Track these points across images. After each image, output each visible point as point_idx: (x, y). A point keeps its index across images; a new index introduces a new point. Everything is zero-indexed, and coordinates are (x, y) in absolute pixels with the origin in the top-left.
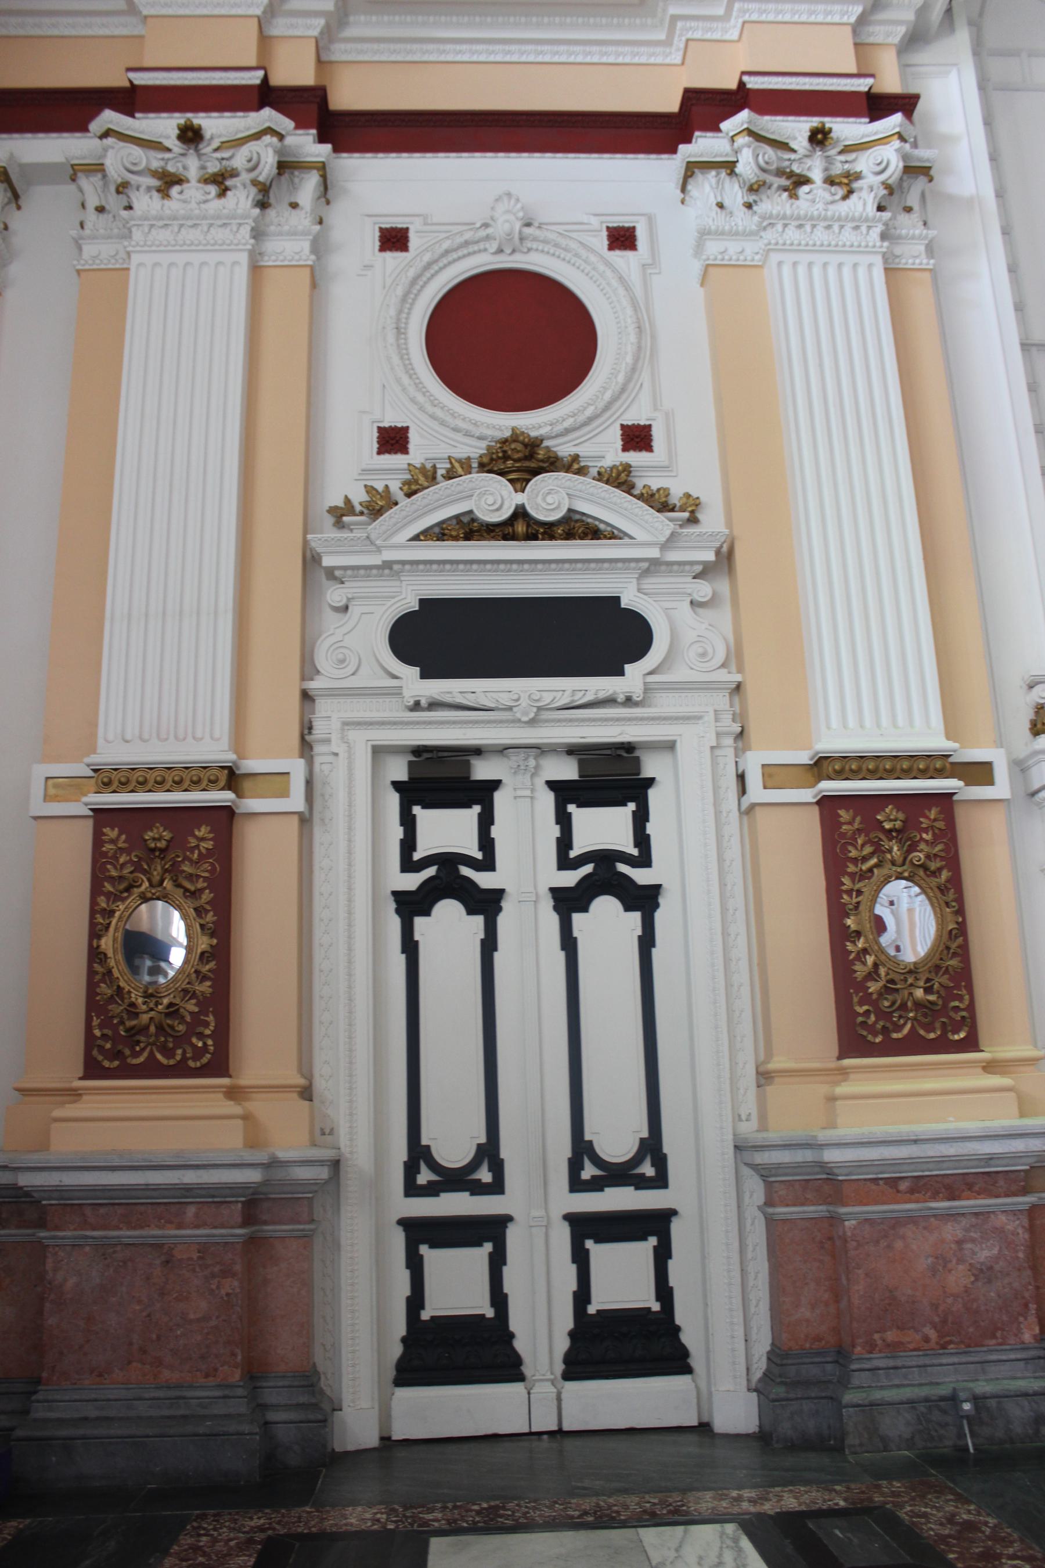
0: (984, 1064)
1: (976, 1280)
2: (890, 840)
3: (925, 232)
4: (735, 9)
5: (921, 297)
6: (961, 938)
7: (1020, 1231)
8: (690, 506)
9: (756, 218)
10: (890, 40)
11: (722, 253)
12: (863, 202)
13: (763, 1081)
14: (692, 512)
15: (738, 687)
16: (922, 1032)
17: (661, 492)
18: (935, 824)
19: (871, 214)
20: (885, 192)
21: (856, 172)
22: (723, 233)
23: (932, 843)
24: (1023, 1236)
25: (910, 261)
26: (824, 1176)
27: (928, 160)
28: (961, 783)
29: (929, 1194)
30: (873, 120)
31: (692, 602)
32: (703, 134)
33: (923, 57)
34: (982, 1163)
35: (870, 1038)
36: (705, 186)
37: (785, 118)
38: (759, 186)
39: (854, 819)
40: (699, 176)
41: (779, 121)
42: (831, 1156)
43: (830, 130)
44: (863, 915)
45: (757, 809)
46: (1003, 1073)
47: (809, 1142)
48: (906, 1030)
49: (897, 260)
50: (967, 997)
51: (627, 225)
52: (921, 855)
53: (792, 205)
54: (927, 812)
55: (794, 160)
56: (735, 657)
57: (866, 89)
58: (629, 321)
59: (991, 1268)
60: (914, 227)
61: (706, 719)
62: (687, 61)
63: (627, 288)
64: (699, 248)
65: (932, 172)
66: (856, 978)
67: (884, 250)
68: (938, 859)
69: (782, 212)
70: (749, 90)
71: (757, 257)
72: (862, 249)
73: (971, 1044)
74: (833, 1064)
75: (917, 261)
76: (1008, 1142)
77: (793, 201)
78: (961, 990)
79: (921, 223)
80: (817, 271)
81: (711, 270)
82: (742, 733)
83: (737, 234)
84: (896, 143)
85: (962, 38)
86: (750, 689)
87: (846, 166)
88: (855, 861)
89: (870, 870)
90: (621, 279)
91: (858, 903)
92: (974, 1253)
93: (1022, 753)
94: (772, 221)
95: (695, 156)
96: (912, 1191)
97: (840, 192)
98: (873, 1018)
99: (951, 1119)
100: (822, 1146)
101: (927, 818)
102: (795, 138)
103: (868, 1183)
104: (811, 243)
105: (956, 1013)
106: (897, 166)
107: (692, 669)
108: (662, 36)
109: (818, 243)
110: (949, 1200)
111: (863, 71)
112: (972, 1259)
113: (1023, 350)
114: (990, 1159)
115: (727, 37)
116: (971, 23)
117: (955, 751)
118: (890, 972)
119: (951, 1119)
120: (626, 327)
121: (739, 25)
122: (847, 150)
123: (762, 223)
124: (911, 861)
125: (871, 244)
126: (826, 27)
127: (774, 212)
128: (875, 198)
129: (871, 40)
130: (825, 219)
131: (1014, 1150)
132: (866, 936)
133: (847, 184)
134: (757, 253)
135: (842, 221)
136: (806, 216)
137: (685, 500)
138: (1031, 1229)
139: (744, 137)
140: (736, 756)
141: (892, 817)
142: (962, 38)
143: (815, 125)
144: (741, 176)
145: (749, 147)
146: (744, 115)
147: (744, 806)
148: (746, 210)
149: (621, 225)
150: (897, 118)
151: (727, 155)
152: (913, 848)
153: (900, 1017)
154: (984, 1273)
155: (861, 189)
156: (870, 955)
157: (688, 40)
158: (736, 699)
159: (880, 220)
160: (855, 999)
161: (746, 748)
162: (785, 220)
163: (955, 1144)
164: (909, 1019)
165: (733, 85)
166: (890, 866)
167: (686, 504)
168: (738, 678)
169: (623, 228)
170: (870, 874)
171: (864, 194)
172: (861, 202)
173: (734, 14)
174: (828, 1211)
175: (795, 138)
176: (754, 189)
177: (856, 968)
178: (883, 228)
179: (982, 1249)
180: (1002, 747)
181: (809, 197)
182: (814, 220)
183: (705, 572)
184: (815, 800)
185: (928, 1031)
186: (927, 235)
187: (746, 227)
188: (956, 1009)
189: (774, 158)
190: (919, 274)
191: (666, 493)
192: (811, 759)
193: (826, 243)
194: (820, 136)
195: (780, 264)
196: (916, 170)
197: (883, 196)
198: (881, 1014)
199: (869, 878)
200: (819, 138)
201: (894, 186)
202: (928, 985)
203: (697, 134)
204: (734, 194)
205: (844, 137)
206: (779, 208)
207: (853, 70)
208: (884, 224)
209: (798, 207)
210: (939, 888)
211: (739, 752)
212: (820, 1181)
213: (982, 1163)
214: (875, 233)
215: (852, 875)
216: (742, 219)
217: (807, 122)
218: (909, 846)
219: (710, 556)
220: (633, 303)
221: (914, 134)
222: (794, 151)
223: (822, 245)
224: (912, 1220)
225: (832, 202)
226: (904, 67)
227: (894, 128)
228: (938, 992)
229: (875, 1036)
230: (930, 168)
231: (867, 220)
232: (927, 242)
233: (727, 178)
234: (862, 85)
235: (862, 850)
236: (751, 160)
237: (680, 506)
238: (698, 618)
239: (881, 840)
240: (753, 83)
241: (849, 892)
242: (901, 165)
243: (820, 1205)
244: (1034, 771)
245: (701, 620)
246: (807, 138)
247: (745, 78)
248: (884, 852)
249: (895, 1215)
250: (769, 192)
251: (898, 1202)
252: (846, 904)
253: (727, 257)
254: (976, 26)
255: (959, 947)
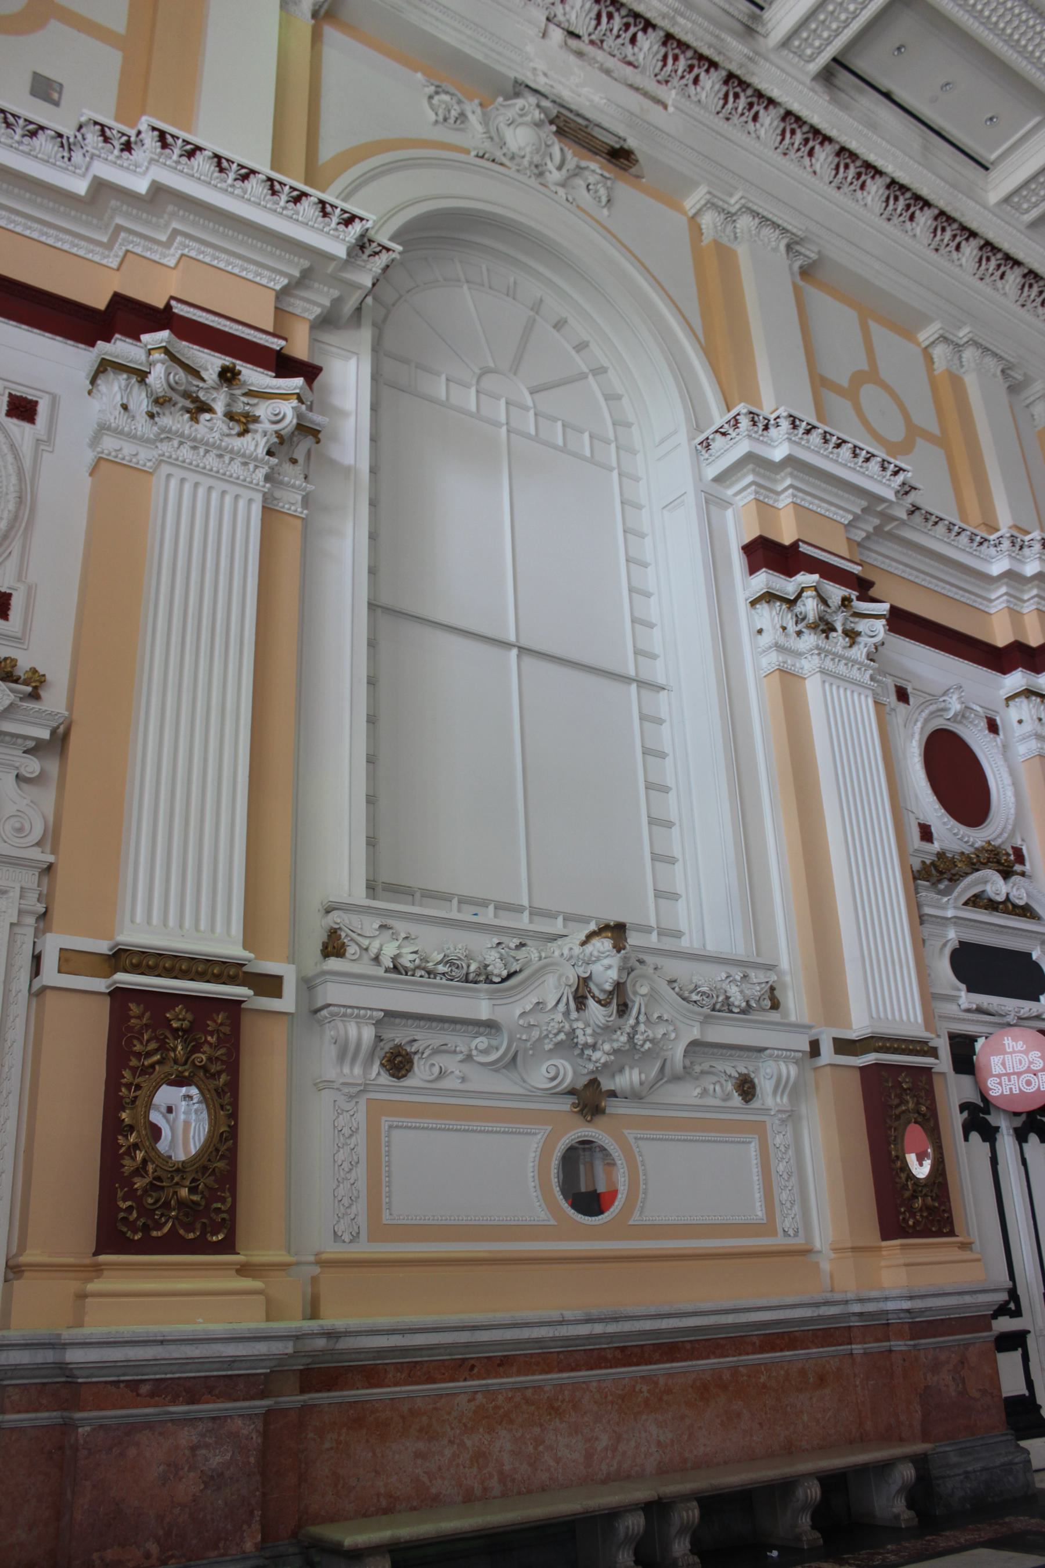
0: (239, 1267)
1: (206, 1487)
2: (176, 1039)
3: (304, 484)
4: (177, 241)
5: (290, 539)
6: (232, 1141)
7: (254, 1435)
8: (35, 681)
9: (156, 429)
10: (306, 315)
11: (116, 451)
12: (255, 444)
13: (11, 1275)
14: (35, 688)
15: (49, 869)
16: (182, 1232)
17: (8, 662)
18: (221, 1028)
19: (260, 456)
20: (276, 440)
21: (254, 416)
22: (121, 433)
23: (216, 1046)
24: (257, 1439)
25: (287, 506)
26: (63, 1379)
27: (318, 424)
28: (251, 992)
29: (169, 1398)
30: (278, 376)
31: (17, 776)
32: (123, 338)
33: (332, 338)
34: (226, 1366)
35: (129, 1234)
36: (114, 387)
37: (202, 349)
38: (165, 401)
39: (143, 1014)
40: (111, 374)
41: (196, 350)
42: (74, 1356)
43: (239, 373)
44: (140, 1109)
45: (48, 992)
46: (254, 1277)
47: (52, 1341)
48: (166, 1229)
49: (275, 502)
50: (229, 1200)
51: (30, 397)
52: (204, 1057)
53: (191, 427)
54: (215, 1015)
55: (202, 388)
56: (52, 838)
57: (278, 348)
58: (12, 489)
59: (222, 1474)
60: (296, 478)
61: (11, 894)
62: (124, 267)
63: (17, 457)
64: (95, 440)
65: (320, 436)
66: (123, 1173)
67: (266, 490)
68: (219, 1063)
69: (181, 431)
70: (175, 314)
71: (149, 464)
72: (185, 465)
73: (228, 1246)
74: (89, 1260)
75: (293, 508)
76: (253, 1344)
77: (193, 423)
78: (224, 1192)
79: (302, 476)
80: (201, 492)
81: (102, 463)
82: (45, 913)
83: (135, 437)
84: (295, 403)
85: (365, 335)
86: (61, 872)
87: (247, 408)
88: (138, 1055)
89: (152, 1066)
90: (12, 446)
91: (136, 1097)
92: (207, 1459)
93: (310, 971)
94: (169, 436)
95: (110, 355)
96: (152, 1394)
97: (237, 429)
98: (135, 1214)
99: (200, 1320)
100: (65, 1346)
101: (215, 1021)
102: (207, 370)
103: (109, 1386)
104: (201, 465)
105: (217, 1215)
106: (291, 422)
107: (5, 842)
108: (105, 239)
109: (208, 467)
110: (188, 1403)
111: (277, 333)
112: (204, 1465)
113: (369, 608)
114: (234, 1361)
115: (165, 261)
116: (374, 325)
117: (250, 961)
118: (158, 1169)
119: (200, 1320)
120: (7, 494)
121: (178, 256)
122: (250, 394)
123: (160, 434)
124: (193, 1061)
125: (255, 482)
126: (251, 283)
127: (174, 428)
128: (266, 443)
129: (290, 309)
130: (219, 447)
131: (256, 1353)
132: (138, 1131)
133: (245, 424)
134: (150, 460)
135: (234, 454)
136: (202, 440)
137: (30, 674)
138: (265, 1434)
139: (160, 354)
140: (35, 936)
141: (180, 1017)
142: (365, 335)
143: (227, 363)
144: (150, 386)
145: (163, 363)
146: (165, 334)
147: (35, 989)
148: (148, 418)
149: (24, 395)
150: (299, 381)
151: (141, 364)
152: (196, 1049)
153: (162, 1215)
154: (215, 1480)
155: (256, 431)
156: (141, 1151)
157: (127, 251)
158: (45, 880)
159: (267, 463)
160: (120, 1194)
161: (47, 929)
162: (183, 439)
163: (201, 1346)
164: (170, 1217)
165: (161, 304)
166: (172, 1064)
167: (31, 678)
168: (51, 859)
169: (25, 399)
170: (151, 1070)
171: (258, 436)
172: (254, 443)
173: (175, 244)
174: (63, 1418)
175: (207, 370)
176: (161, 402)
177: (125, 1162)
178: (269, 471)
179: (215, 1456)
180: (293, 964)
181: (209, 424)
182: (209, 447)
183: (37, 749)
184: (108, 991)
185: (188, 1231)
186: (306, 487)
187: (144, 434)
188: (218, 1210)
189: (184, 380)
190: (290, 519)
191: (13, 663)
192: (111, 950)
193: (215, 469)
194: (229, 375)
195: (169, 476)
196: (306, 430)
197: (275, 443)
198: (143, 1211)
199: (150, 1074)
200: (228, 376)
201: (285, 438)
202: (193, 1184)
203: (117, 336)
204: (141, 402)
205: (250, 382)
206: (179, 426)
207: (271, 329)
208: (270, 468)
209: (196, 430)
210: (216, 1090)
211: (38, 933)
212: (58, 1385)
213: (226, 1366)
214: (260, 474)
215: (134, 1070)
216: (142, 426)
217: (221, 358)
218: (193, 1046)
219: (45, 734)
220: (19, 473)
221: (311, 399)
222: (203, 380)
223: (211, 470)
224: (148, 1425)
225: (228, 435)
226: (313, 341)
227: (294, 389)
228: (202, 1193)
229: (135, 1232)
230: (319, 431)
231: (256, 459)
232: (304, 493)
233: (137, 385)
234: (276, 344)
235: (146, 1045)
236: (162, 375)
237: (25, 680)
238: (19, 791)
239: (166, 1037)
240: (178, 309)
241: (128, 1086)
242: (295, 421)
243: (55, 1410)
244: (320, 989)
245: (24, 795)
246: (217, 372)
247: (173, 303)
248: (168, 1050)
249: (131, 1420)
250: (173, 408)
251: (137, 1407)
252: (122, 1098)
253: (120, 456)
254: (379, 329)
255: (228, 1149)
